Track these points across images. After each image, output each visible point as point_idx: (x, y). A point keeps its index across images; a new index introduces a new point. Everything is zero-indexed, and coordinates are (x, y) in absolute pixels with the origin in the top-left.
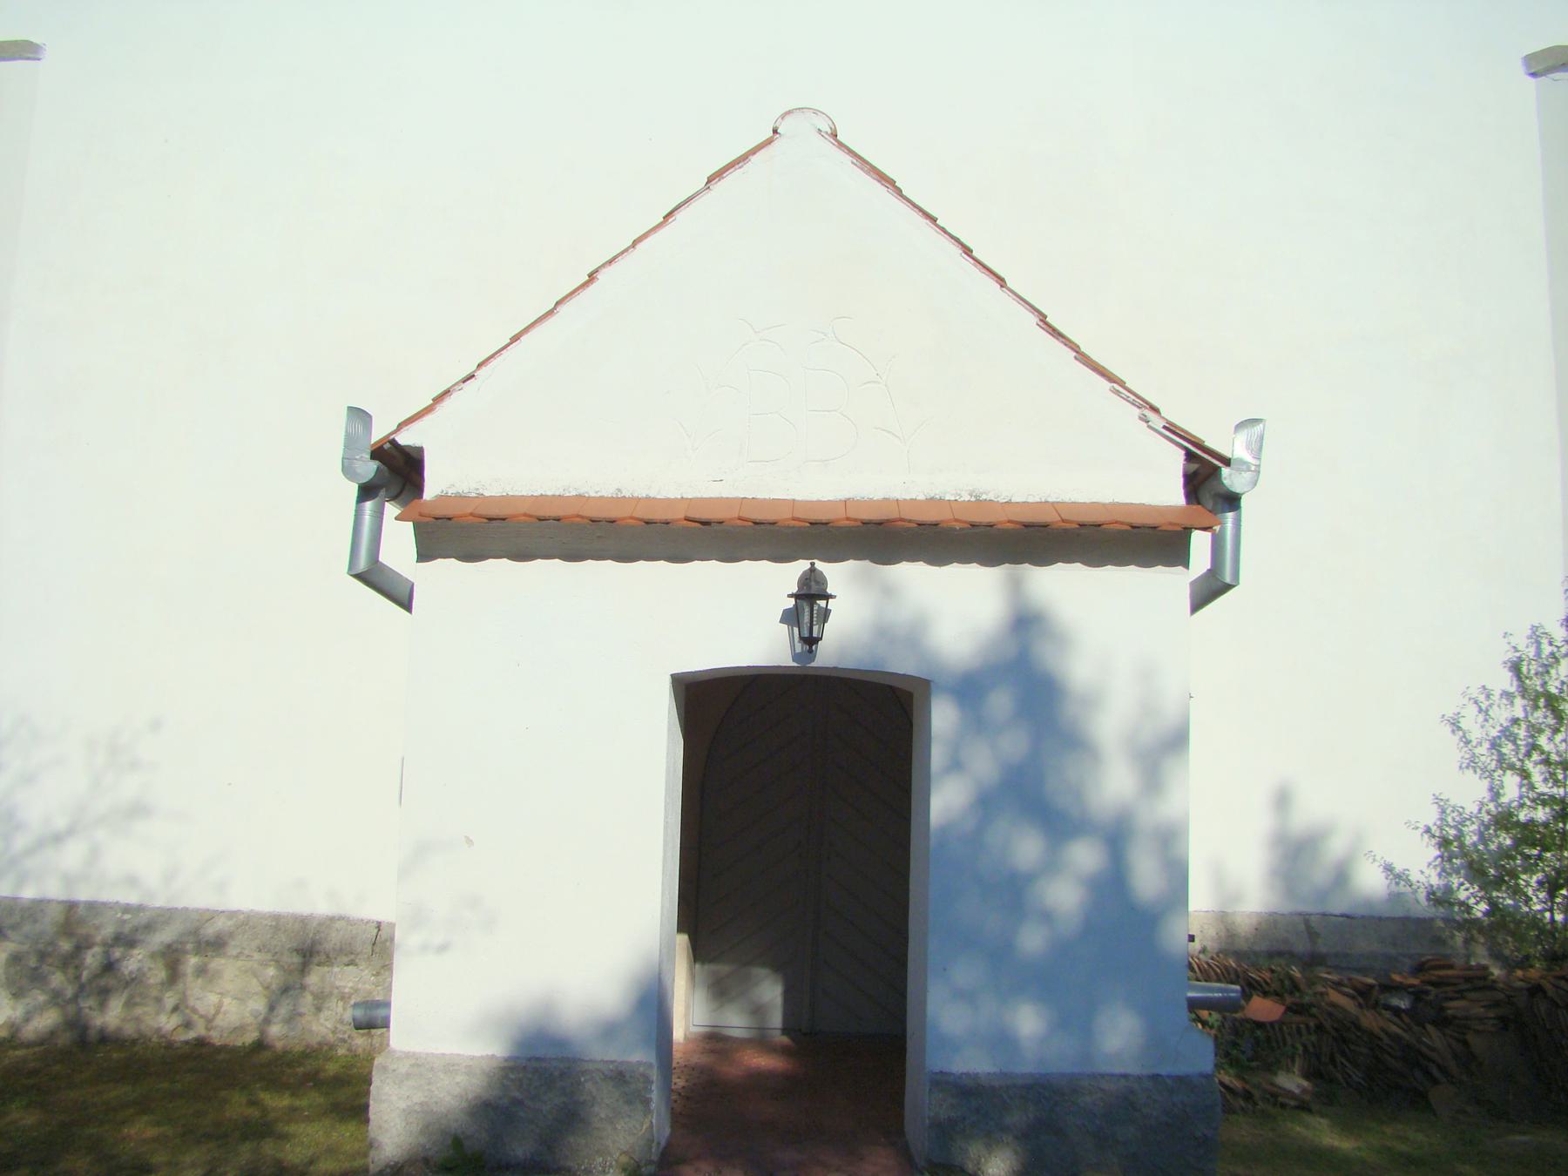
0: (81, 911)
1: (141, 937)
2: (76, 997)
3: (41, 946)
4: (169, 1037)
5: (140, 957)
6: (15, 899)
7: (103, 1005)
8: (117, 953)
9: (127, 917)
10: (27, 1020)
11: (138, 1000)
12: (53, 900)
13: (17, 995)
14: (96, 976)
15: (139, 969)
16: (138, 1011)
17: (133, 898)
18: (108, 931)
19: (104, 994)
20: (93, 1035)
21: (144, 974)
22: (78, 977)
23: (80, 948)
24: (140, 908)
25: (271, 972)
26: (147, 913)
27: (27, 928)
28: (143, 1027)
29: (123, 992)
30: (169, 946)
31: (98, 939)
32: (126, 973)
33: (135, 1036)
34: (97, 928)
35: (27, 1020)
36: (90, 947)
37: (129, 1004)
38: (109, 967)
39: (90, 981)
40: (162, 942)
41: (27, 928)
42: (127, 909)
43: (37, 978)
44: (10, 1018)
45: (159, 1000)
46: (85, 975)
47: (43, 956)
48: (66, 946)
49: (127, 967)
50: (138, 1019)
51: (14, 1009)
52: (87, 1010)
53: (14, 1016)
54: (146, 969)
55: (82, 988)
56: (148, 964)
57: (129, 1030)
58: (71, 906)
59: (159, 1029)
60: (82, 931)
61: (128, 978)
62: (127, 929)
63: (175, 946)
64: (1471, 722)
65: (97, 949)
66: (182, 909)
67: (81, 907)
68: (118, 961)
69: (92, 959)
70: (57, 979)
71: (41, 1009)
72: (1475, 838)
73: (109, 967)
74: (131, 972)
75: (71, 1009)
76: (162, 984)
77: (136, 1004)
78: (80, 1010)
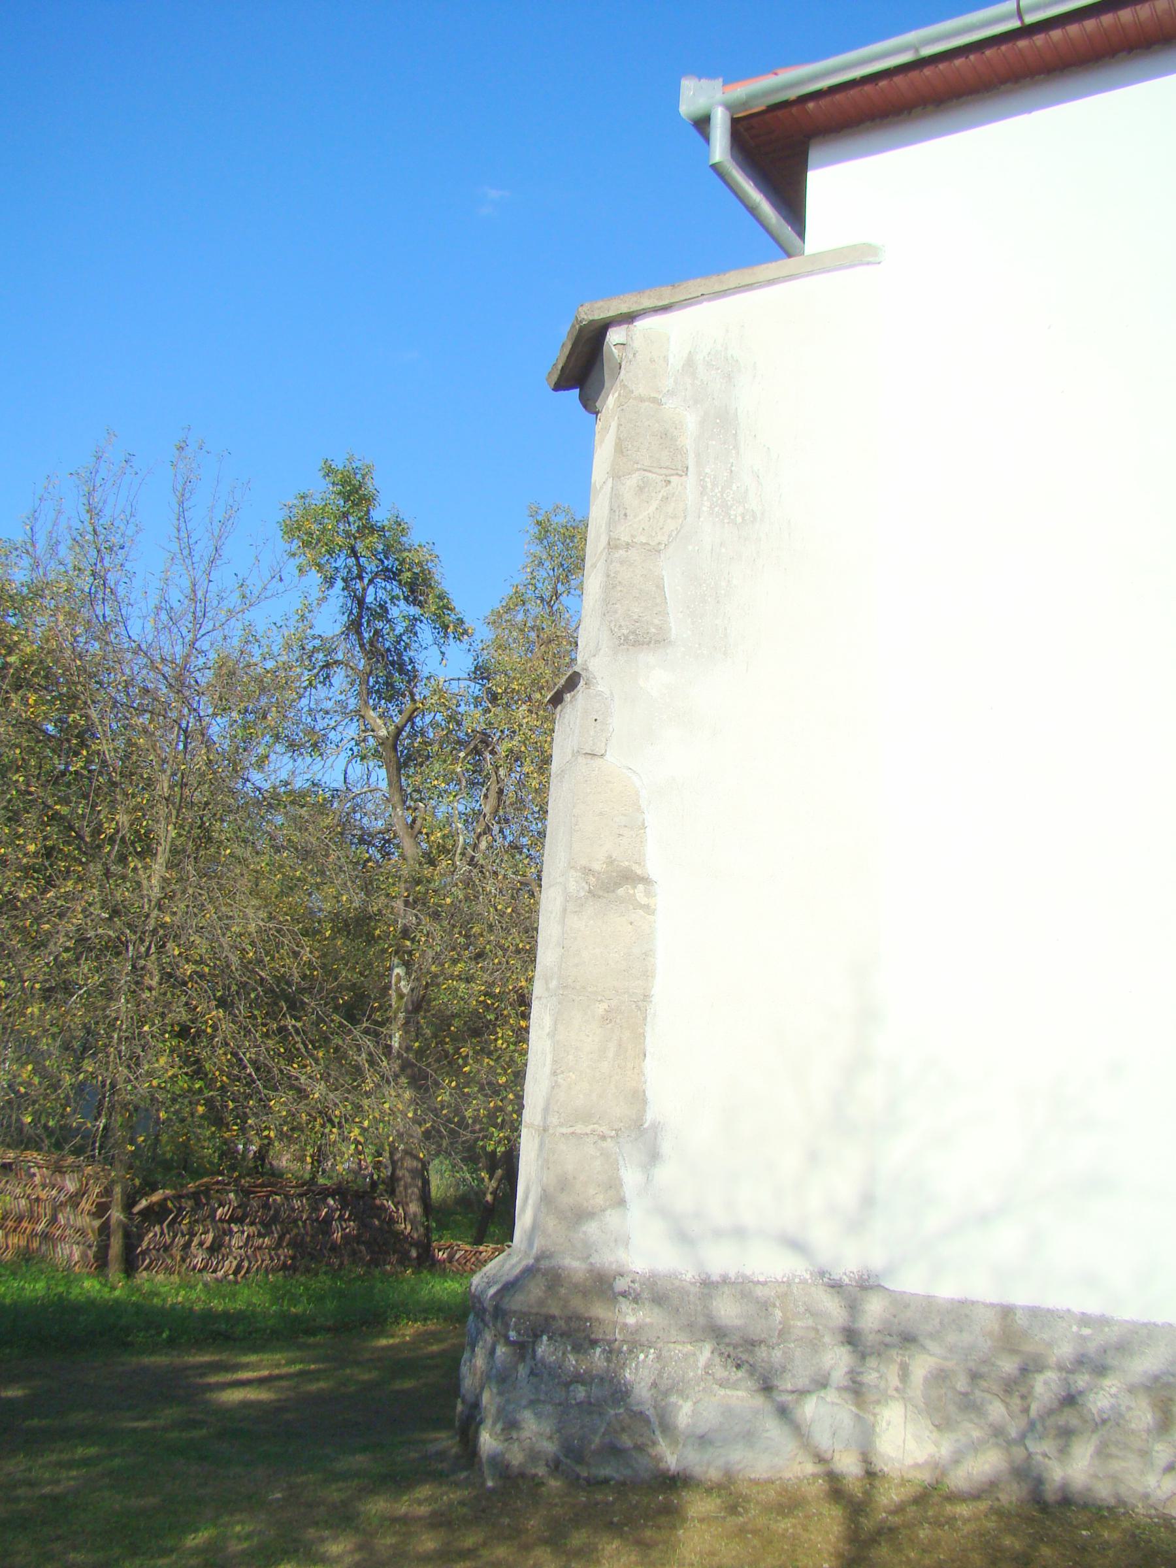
0: (1021, 1320)
1: (1115, 1363)
2: (1023, 1436)
3: (972, 1365)
4: (1161, 1509)
5: (1113, 1390)
6: (929, 1298)
7: (1064, 1452)
8: (1082, 1380)
9: (1086, 1331)
10: (957, 1461)
11: (1113, 1450)
12: (978, 1302)
13: (943, 1425)
14: (1051, 1412)
15: (1112, 1407)
16: (1115, 1466)
17: (1091, 1305)
18: (1065, 1350)
19: (1066, 1434)
20: (1050, 1496)
21: (1121, 1416)
22: (1026, 1410)
23: (1030, 1368)
24: (1103, 1321)
25: (1133, 1426)
26: (1116, 1328)
27: (951, 1338)
28: (1123, 1490)
29: (1090, 1438)
30: (1156, 1378)
31: (1052, 1360)
32: (1094, 1411)
33: (1112, 1502)
34: (1050, 1345)
35: (957, 1461)
36: (1040, 1369)
37: (1102, 1453)
38: (1070, 1400)
39: (1042, 1418)
40: (1145, 1372)
41: (951, 1338)
42: (1085, 1320)
43: (969, 1406)
44: (932, 1456)
45: (1144, 1454)
46: (1034, 1408)
47: (975, 1376)
48: (1008, 1366)
49: (1095, 1402)
50: (1115, 1479)
51: (937, 1444)
52: (1040, 1458)
53: (937, 1455)
54: (1123, 1408)
55: (1032, 1425)
56: (1126, 1400)
57: (1104, 1492)
58: (1006, 1312)
59: (1146, 1496)
60: (1029, 1348)
61: (1098, 1419)
62: (1092, 1347)
63: (1165, 1379)
64: (377, 505)
65: (1051, 1375)
66: (1163, 1324)
67: (1019, 1313)
68: (1081, 1393)
69: (1045, 1387)
70: (996, 1410)
71: (975, 1447)
72: (147, 1287)
73: (1070, 1400)
74: (1101, 1411)
75: (1019, 1453)
76: (1149, 1431)
77: (1110, 1456)
78: (1030, 1456)
